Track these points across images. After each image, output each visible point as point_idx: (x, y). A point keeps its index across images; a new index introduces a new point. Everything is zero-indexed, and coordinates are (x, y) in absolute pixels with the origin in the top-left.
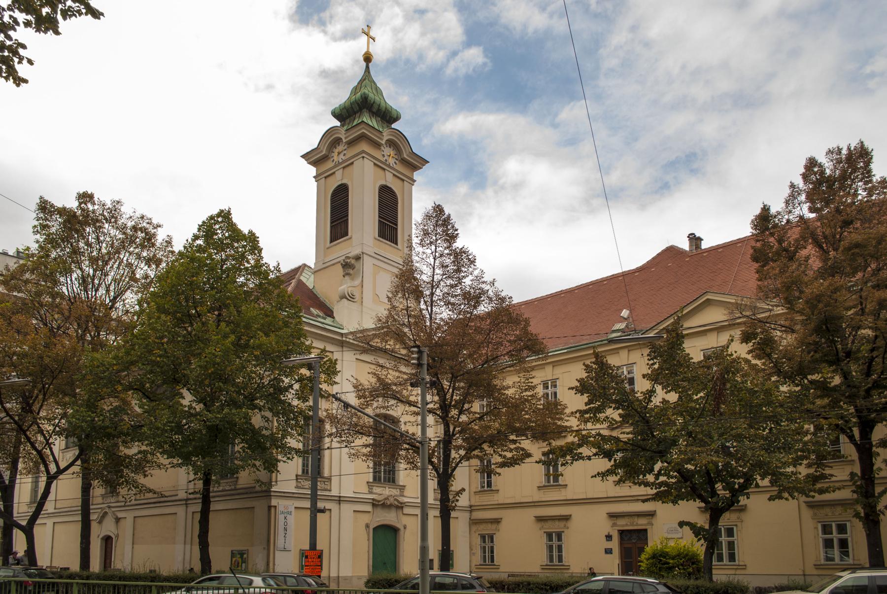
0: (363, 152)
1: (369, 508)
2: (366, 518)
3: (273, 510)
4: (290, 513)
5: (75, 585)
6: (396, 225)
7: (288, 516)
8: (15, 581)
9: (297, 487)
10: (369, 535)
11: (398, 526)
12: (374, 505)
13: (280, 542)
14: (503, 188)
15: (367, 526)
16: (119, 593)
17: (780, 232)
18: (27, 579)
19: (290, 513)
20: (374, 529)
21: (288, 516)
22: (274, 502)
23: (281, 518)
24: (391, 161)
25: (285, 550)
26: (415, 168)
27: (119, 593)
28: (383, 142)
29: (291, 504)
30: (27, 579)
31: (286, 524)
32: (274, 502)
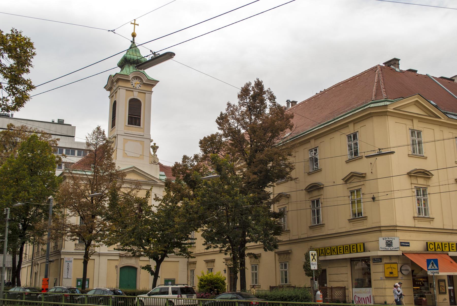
0: (119, 86)
1: (117, 258)
2: (116, 263)
3: (62, 260)
4: (71, 262)
5: (280, 304)
6: (140, 116)
7: (70, 263)
8: (237, 302)
9: (76, 249)
10: (117, 271)
11: (136, 266)
12: (120, 256)
13: (65, 275)
14: (35, 87)
15: (116, 267)
16: (225, 305)
17: (13, 67)
18: (126, 296)
19: (71, 262)
20: (121, 268)
21: (70, 263)
22: (62, 257)
23: (65, 264)
24: (137, 86)
25: (68, 278)
26: (153, 86)
27: (225, 305)
28: (130, 79)
29: (72, 257)
30: (126, 296)
31: (68, 266)
32: (62, 257)
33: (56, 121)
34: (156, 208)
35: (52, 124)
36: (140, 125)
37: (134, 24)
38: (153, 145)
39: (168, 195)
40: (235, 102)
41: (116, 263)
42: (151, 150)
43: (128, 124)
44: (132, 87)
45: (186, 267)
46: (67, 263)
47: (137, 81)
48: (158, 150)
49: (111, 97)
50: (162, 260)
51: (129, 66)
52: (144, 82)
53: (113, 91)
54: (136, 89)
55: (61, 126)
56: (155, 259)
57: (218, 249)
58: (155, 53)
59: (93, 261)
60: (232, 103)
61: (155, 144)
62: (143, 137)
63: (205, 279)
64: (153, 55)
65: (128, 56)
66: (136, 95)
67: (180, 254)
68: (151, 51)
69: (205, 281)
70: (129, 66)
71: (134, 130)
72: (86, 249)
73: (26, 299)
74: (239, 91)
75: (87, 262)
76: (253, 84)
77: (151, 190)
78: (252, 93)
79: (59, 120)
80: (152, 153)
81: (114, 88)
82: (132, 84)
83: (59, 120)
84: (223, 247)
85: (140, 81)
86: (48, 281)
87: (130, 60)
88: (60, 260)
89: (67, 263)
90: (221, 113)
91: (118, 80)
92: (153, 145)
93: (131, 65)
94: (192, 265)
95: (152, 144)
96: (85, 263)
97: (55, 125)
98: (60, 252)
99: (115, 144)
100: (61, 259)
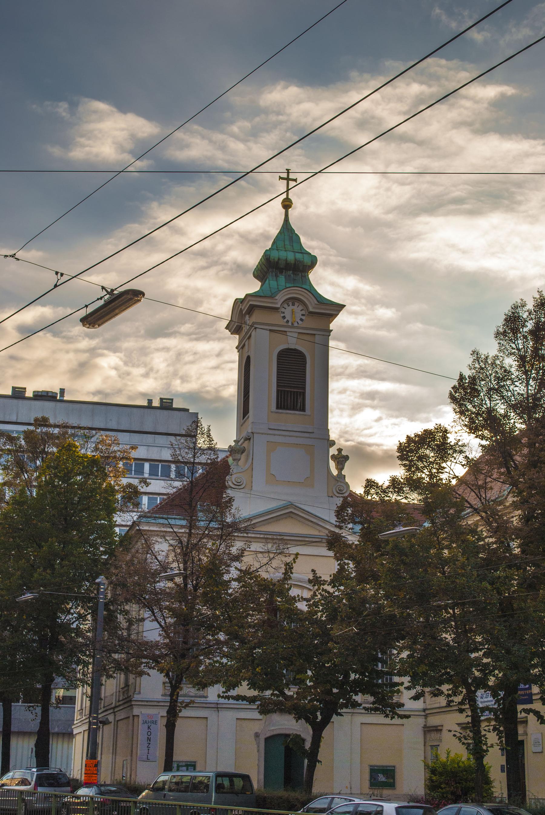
4: (155, 722)
7: (153, 726)
15: (257, 735)
20: (267, 739)
28: (278, 306)
31: (149, 733)
33: (156, 403)
34: (305, 603)
35: (146, 410)
36: (303, 409)
37: (288, 179)
38: (336, 453)
39: (342, 569)
40: (491, 348)
41: (257, 727)
42: (332, 465)
43: (278, 408)
44: (283, 322)
45: (421, 740)
46: (146, 726)
47: (298, 309)
48: (347, 464)
49: (240, 348)
50: (326, 721)
51: (277, 276)
52: (311, 309)
53: (243, 333)
54: (293, 326)
55: (165, 412)
56: (311, 722)
57: (442, 701)
58: (112, 290)
59: (204, 720)
60: (483, 352)
61: (340, 450)
62: (312, 435)
63: (440, 770)
64: (108, 296)
65: (275, 255)
66: (292, 341)
67: (376, 709)
68: (103, 288)
69: (441, 774)
70: (277, 276)
71: (291, 419)
72: (171, 695)
73: (215, 803)
74: (499, 322)
75: (174, 726)
76: (530, 306)
77: (295, 562)
78: (530, 325)
79: (161, 399)
80: (335, 472)
81: (245, 328)
82: (284, 317)
83: (161, 399)
84: (455, 694)
85: (301, 307)
86: (96, 766)
87: (277, 262)
88: (131, 718)
89: (146, 726)
90: (461, 375)
91: (251, 309)
92: (336, 453)
93: (281, 273)
94: (434, 735)
95: (333, 451)
96: (170, 727)
97: (152, 411)
98: (131, 701)
99: (248, 456)
100: (134, 716)
